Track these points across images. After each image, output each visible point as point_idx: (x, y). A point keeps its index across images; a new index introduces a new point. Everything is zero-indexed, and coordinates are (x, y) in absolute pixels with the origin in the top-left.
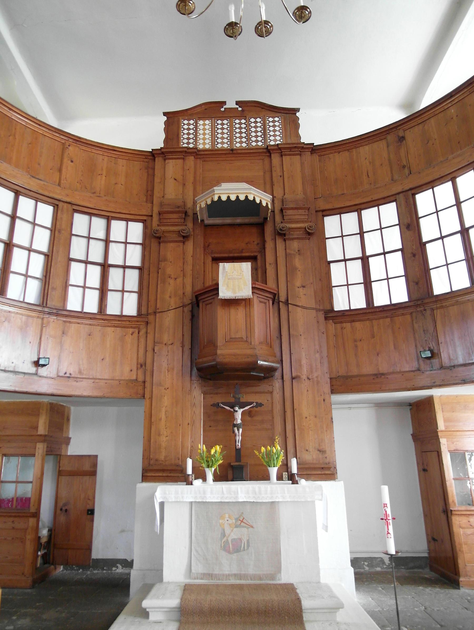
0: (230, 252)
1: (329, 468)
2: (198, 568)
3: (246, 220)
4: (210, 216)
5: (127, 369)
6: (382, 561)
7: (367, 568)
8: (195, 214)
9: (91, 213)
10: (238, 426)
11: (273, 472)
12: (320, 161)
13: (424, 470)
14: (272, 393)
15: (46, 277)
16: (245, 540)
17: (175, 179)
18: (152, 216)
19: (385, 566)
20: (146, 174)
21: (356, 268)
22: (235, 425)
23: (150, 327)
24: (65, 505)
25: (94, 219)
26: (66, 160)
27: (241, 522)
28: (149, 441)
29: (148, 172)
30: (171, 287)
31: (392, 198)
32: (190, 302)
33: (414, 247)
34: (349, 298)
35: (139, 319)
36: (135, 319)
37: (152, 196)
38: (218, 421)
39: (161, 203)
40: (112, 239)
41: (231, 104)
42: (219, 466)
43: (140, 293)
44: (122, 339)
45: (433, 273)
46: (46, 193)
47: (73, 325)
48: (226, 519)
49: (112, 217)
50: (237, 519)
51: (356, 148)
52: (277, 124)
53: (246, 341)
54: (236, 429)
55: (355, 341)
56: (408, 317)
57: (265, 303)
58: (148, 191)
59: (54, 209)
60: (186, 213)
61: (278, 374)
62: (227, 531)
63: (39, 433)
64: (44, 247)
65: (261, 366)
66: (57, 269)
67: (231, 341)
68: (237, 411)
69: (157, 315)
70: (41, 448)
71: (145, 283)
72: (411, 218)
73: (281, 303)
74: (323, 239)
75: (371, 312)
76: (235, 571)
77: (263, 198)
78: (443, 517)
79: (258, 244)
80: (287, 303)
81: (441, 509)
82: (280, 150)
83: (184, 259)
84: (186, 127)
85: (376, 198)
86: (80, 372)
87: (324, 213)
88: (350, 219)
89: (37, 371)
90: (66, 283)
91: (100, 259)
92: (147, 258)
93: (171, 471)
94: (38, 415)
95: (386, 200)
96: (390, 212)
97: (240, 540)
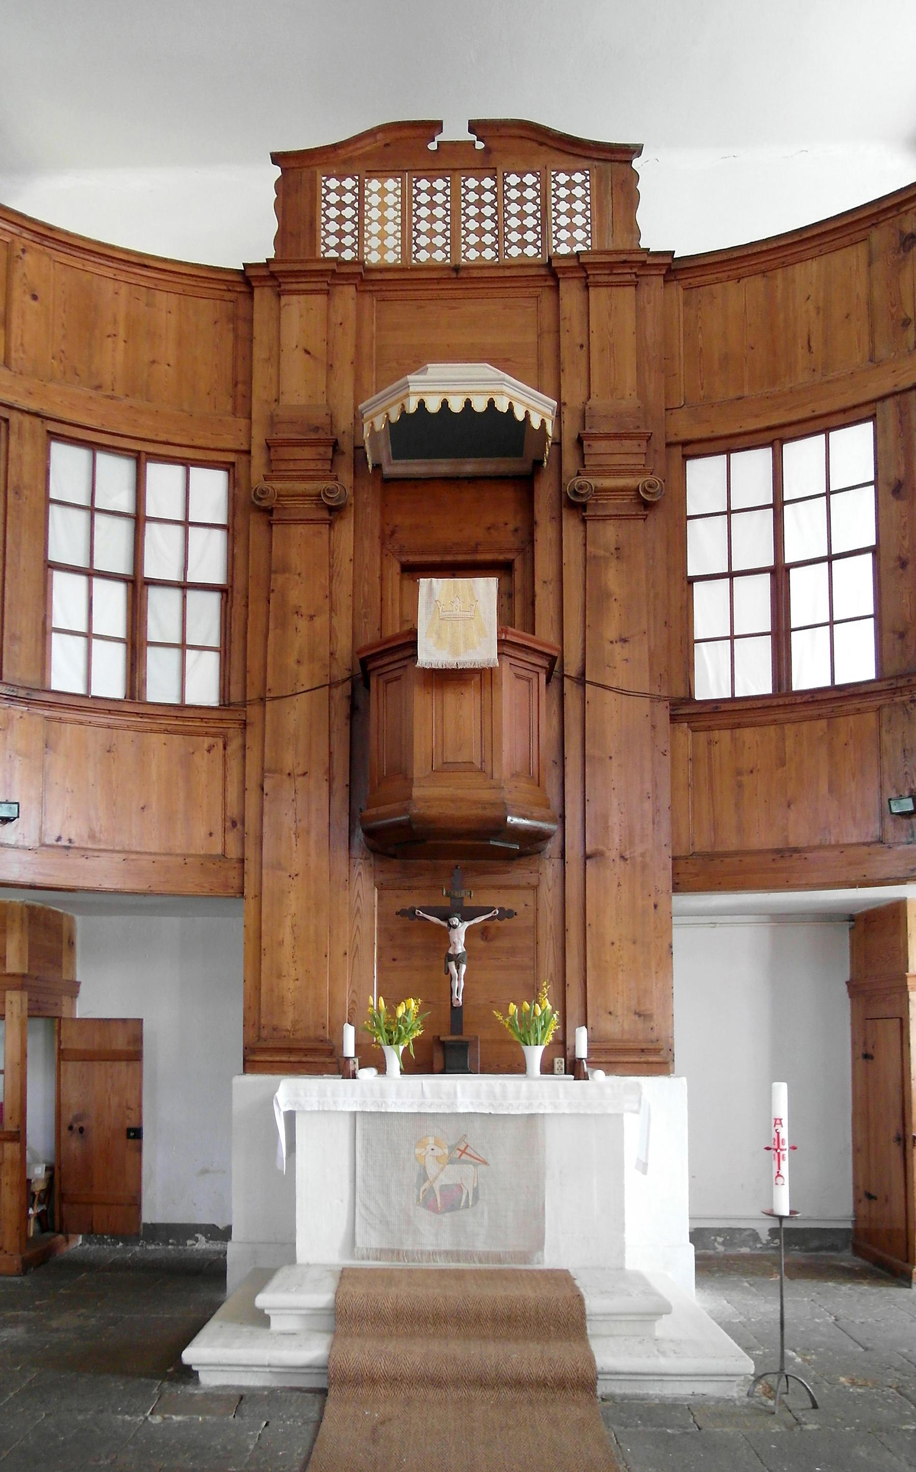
0: (447, 551)
1: (657, 1051)
2: (370, 1239)
3: (489, 466)
4: (398, 454)
5: (201, 831)
7: (721, 1249)
8: (359, 449)
10: (458, 960)
11: (535, 1055)
12: (686, 303)
14: (535, 888)
16: (469, 1187)
18: (248, 452)
19: (759, 1246)
21: (756, 595)
22: (450, 958)
24: (78, 1118)
27: (461, 1152)
28: (258, 988)
29: (235, 330)
30: (300, 636)
31: (866, 411)
32: (347, 674)
35: (225, 715)
36: (215, 714)
37: (248, 397)
39: (272, 417)
41: (456, 131)
43: (225, 652)
44: (187, 762)
48: (429, 1148)
49: (147, 453)
50: (452, 1148)
51: (784, 265)
52: (578, 192)
53: (481, 770)
54: (452, 965)
55: (739, 773)
56: (871, 717)
57: (529, 680)
58: (236, 385)
61: (552, 847)
62: (432, 1169)
63: (9, 970)
65: (515, 828)
67: (444, 769)
68: (455, 927)
74: (680, 520)
76: (446, 1246)
79: (516, 530)
80: (581, 680)
81: (893, 1134)
82: (583, 269)
83: (331, 566)
84: (333, 198)
85: (824, 410)
86: (92, 837)
87: (689, 450)
88: (752, 466)
90: (44, 623)
91: (122, 566)
92: (240, 563)
97: (460, 1187)
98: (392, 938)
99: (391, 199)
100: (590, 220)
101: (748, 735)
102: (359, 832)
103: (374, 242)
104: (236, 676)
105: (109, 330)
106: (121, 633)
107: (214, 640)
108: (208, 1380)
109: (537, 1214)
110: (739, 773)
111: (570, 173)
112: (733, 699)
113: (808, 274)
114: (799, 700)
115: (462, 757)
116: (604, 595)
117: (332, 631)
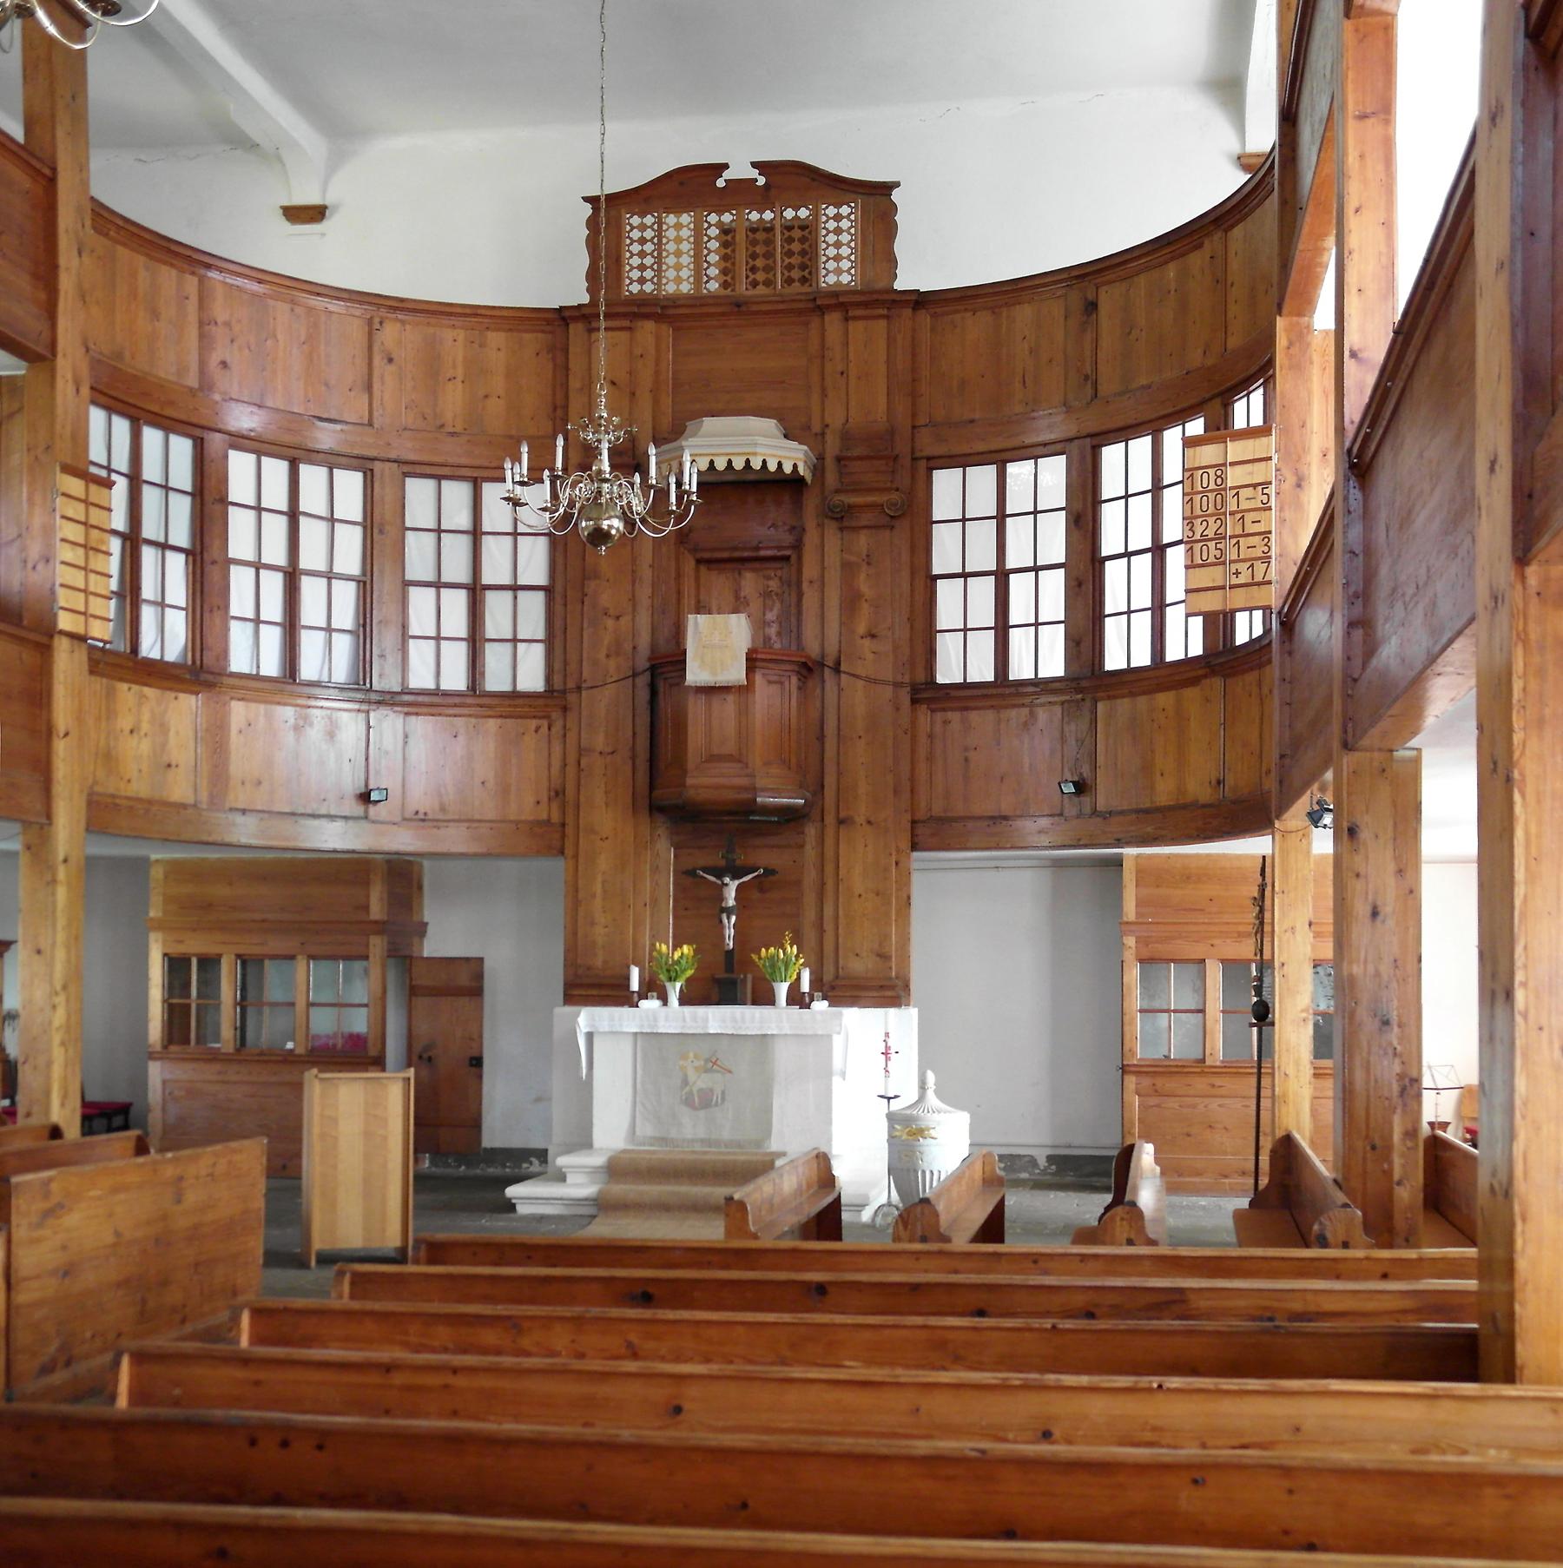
0: (735, 549)
1: (892, 988)
2: (646, 1130)
5: (530, 800)
6: (1033, 1161)
9: (439, 473)
10: (729, 911)
11: (782, 989)
12: (933, 329)
16: (718, 1092)
20: (551, 366)
22: (723, 910)
23: (572, 717)
24: (428, 1048)
26: (378, 360)
27: (712, 1064)
28: (575, 934)
29: (554, 359)
31: (1059, 447)
32: (648, 665)
34: (962, 659)
38: (697, 903)
40: (486, 527)
41: (740, 170)
42: (688, 980)
43: (549, 642)
50: (707, 1061)
52: (845, 224)
54: (724, 916)
55: (966, 749)
56: (1058, 710)
57: (782, 683)
58: (555, 409)
62: (692, 1076)
66: (383, 610)
67: (713, 758)
69: (584, 693)
70: (377, 945)
71: (558, 624)
72: (1085, 500)
77: (788, 456)
80: (837, 669)
82: (842, 303)
84: (636, 234)
86: (443, 809)
87: (932, 464)
88: (983, 477)
89: (366, 812)
91: (464, 576)
92: (560, 567)
94: (366, 884)
96: (1053, 473)
97: (711, 1090)
99: (685, 233)
100: (854, 251)
103: (671, 274)
105: (449, 375)
106: (463, 633)
107: (540, 634)
108: (522, 1209)
109: (768, 1110)
110: (966, 749)
111: (838, 206)
112: (966, 685)
113: (1024, 314)
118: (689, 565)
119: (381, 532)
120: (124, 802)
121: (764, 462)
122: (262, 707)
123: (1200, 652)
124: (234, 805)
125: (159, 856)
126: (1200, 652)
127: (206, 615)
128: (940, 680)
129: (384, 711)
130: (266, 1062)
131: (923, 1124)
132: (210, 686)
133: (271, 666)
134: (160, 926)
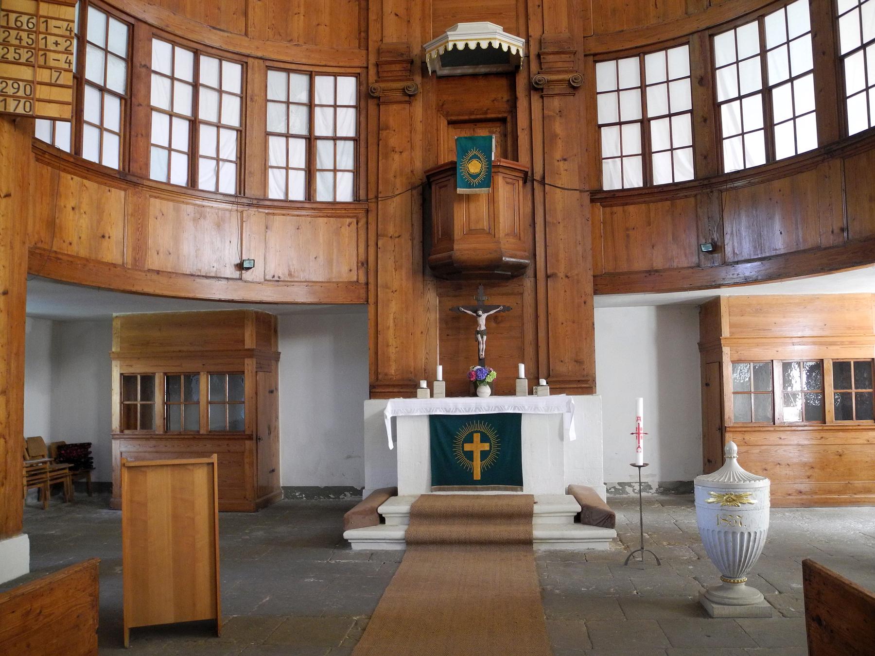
0: (472, 113)
1: (586, 381)
3: (493, 69)
4: (444, 65)
5: (345, 269)
8: (424, 63)
10: (482, 333)
13: (706, 385)
14: (522, 294)
15: (240, 159)
17: (397, 15)
18: (367, 68)
21: (633, 133)
22: (478, 332)
25: (293, 76)
29: (359, 5)
30: (396, 162)
31: (684, 40)
33: (706, 109)
34: (621, 174)
35: (357, 206)
36: (352, 206)
37: (367, 39)
39: (379, 49)
40: (317, 102)
43: (356, 172)
44: (337, 232)
45: (726, 143)
46: (231, 49)
47: (277, 218)
53: (489, 233)
55: (627, 229)
56: (692, 200)
57: (514, 184)
59: (242, 68)
60: (412, 62)
61: (530, 272)
64: (235, 122)
65: (507, 262)
66: (252, 150)
67: (471, 232)
68: (480, 316)
72: (706, 68)
73: (535, 182)
74: (593, 94)
75: (650, 192)
77: (514, 44)
78: (718, 433)
79: (508, 101)
80: (543, 182)
81: (717, 426)
83: (411, 125)
86: (290, 275)
87: (596, 58)
88: (629, 66)
89: (241, 275)
90: (265, 164)
91: (304, 132)
93: (401, 386)
94: (242, 326)
95: (676, 43)
96: (679, 59)
98: (447, 323)
101: (631, 209)
102: (428, 267)
104: (362, 185)
105: (296, 11)
108: (356, 547)
110: (627, 229)
114: (656, 190)
115: (479, 227)
116: (554, 136)
117: (412, 159)
118: (443, 123)
119: (252, 99)
120: (65, 258)
121: (500, 45)
122: (171, 204)
123: (815, 146)
124: (151, 267)
125: (118, 314)
126: (815, 146)
127: (133, 139)
128: (606, 188)
129: (253, 210)
130: (184, 439)
131: (741, 492)
132: (136, 184)
133: (180, 177)
134: (119, 356)
